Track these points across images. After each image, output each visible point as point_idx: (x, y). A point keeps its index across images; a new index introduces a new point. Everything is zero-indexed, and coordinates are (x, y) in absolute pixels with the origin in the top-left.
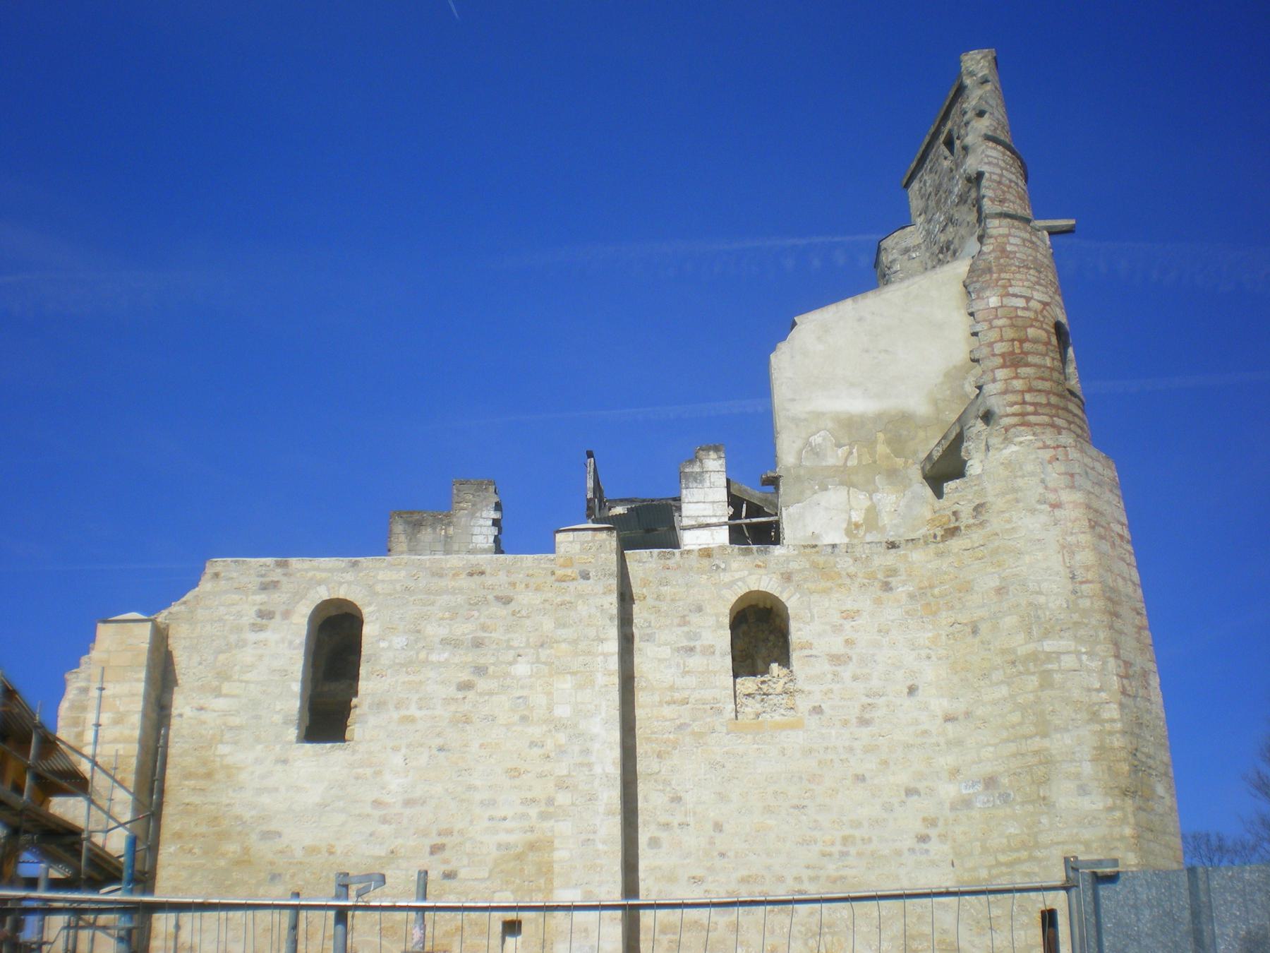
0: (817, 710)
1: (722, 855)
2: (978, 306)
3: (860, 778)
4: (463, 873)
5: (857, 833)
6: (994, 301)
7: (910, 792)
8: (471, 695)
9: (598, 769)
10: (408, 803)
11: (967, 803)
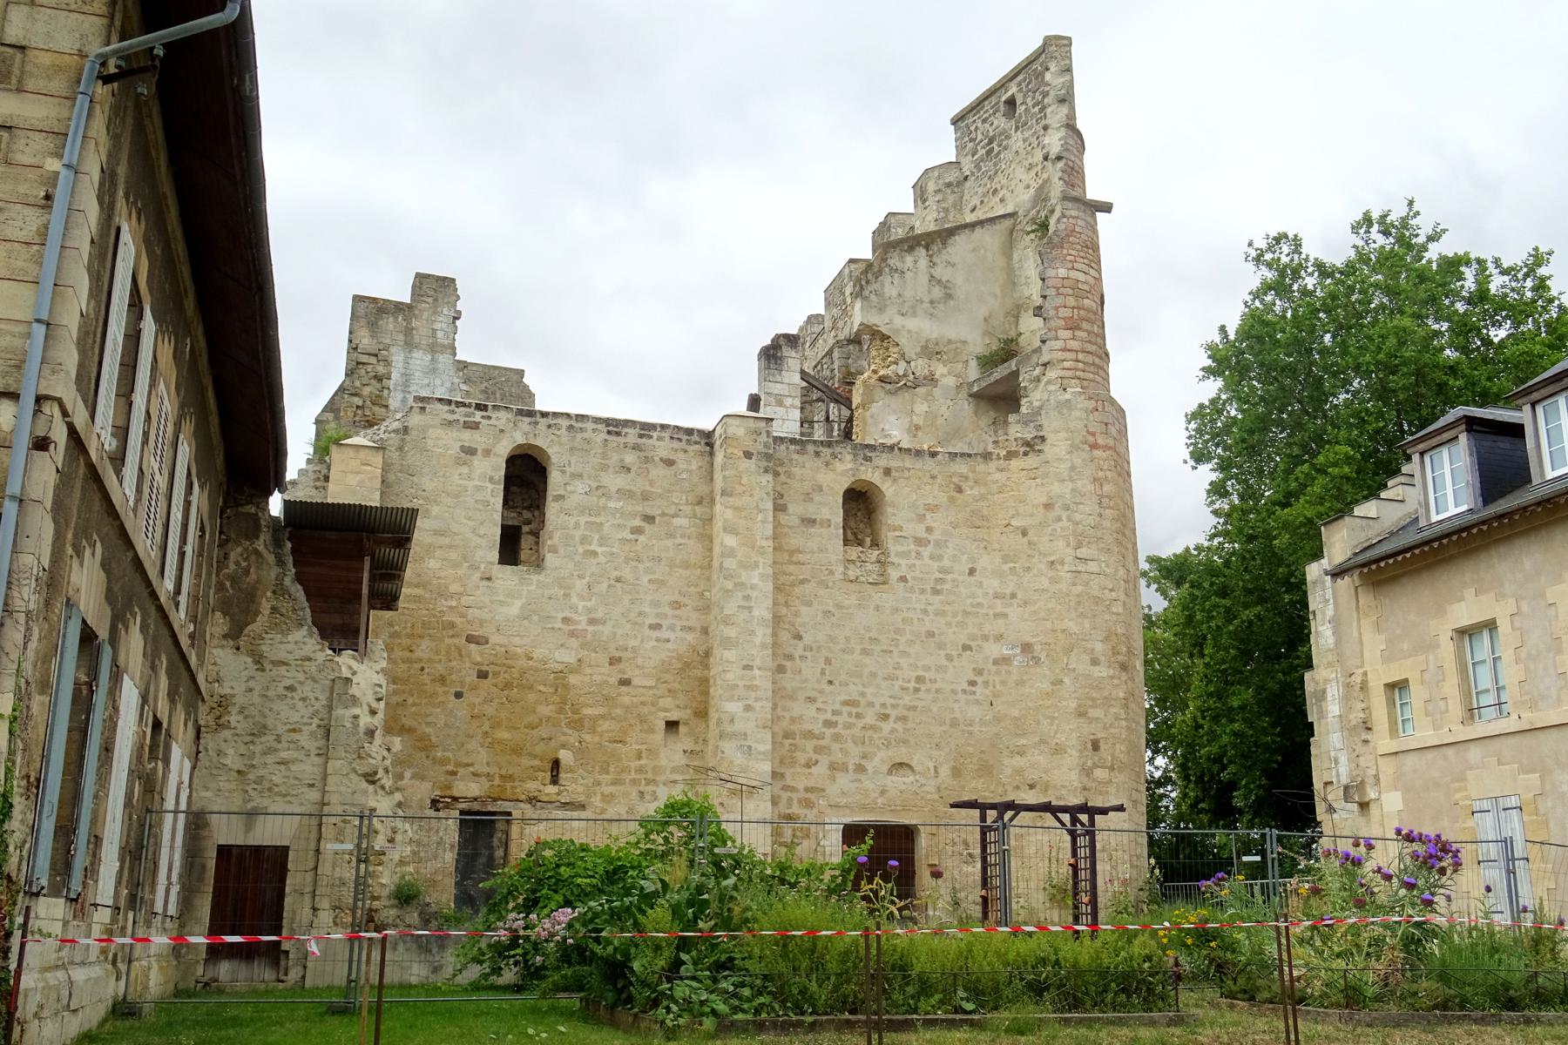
0: (903, 579)
1: (830, 682)
2: (1050, 273)
3: (931, 634)
4: (635, 681)
5: (927, 675)
6: (1062, 272)
7: (966, 648)
8: (642, 538)
9: (756, 613)
10: (592, 622)
11: (1006, 660)
